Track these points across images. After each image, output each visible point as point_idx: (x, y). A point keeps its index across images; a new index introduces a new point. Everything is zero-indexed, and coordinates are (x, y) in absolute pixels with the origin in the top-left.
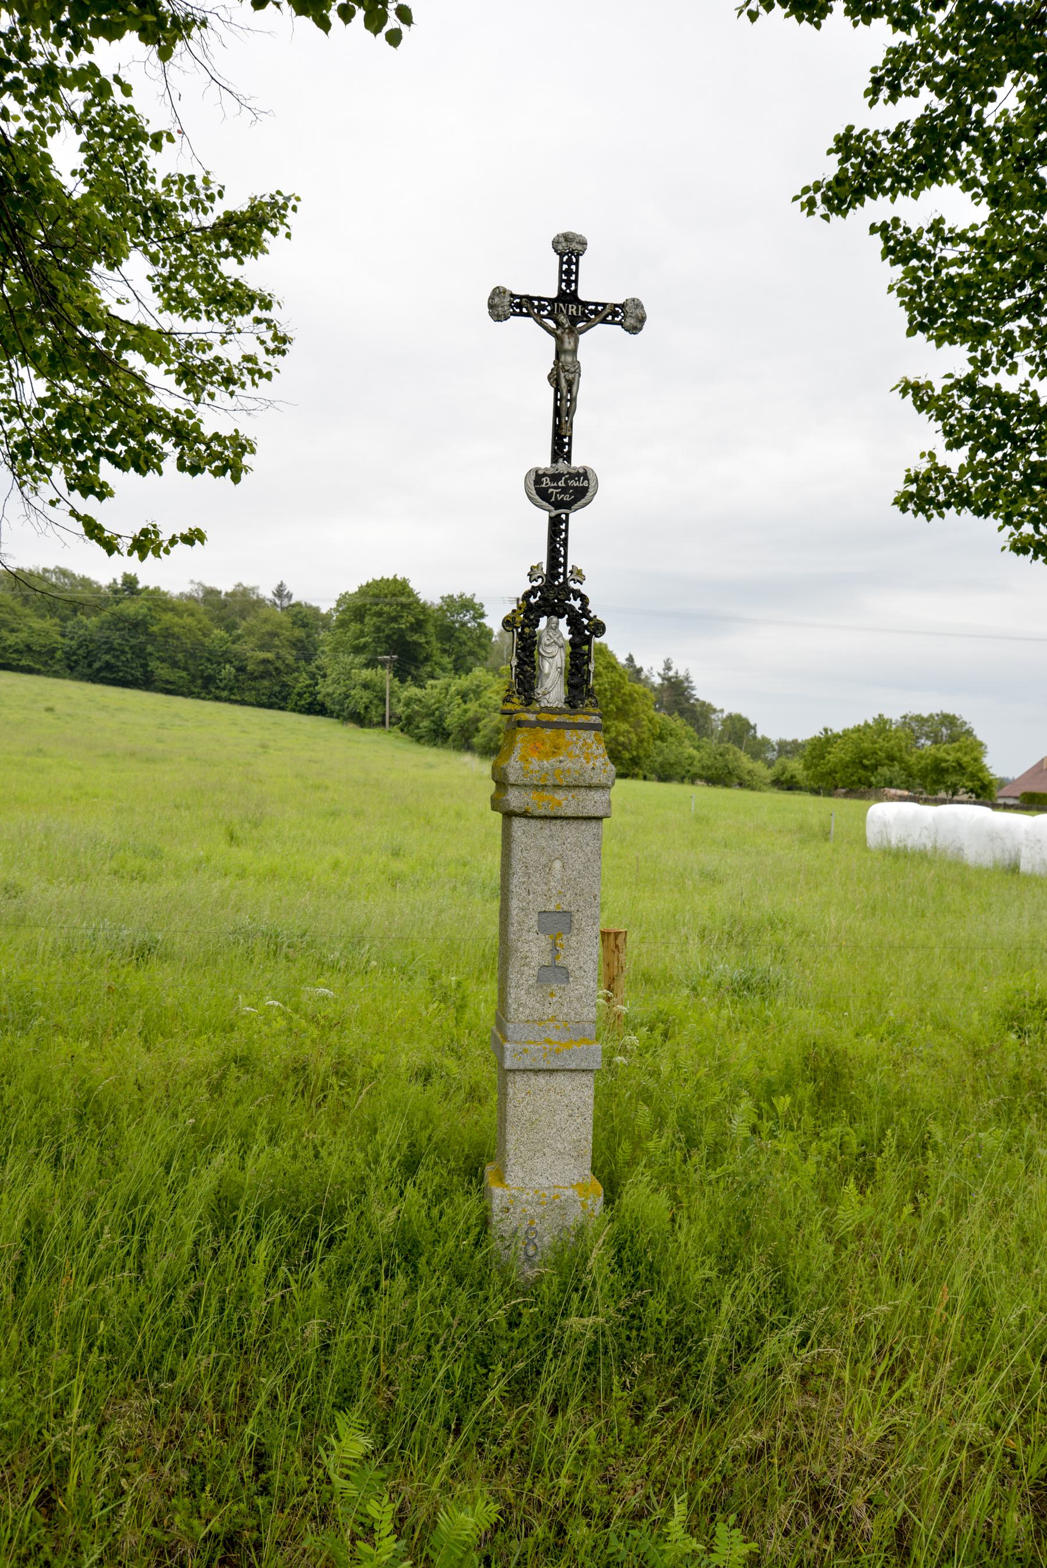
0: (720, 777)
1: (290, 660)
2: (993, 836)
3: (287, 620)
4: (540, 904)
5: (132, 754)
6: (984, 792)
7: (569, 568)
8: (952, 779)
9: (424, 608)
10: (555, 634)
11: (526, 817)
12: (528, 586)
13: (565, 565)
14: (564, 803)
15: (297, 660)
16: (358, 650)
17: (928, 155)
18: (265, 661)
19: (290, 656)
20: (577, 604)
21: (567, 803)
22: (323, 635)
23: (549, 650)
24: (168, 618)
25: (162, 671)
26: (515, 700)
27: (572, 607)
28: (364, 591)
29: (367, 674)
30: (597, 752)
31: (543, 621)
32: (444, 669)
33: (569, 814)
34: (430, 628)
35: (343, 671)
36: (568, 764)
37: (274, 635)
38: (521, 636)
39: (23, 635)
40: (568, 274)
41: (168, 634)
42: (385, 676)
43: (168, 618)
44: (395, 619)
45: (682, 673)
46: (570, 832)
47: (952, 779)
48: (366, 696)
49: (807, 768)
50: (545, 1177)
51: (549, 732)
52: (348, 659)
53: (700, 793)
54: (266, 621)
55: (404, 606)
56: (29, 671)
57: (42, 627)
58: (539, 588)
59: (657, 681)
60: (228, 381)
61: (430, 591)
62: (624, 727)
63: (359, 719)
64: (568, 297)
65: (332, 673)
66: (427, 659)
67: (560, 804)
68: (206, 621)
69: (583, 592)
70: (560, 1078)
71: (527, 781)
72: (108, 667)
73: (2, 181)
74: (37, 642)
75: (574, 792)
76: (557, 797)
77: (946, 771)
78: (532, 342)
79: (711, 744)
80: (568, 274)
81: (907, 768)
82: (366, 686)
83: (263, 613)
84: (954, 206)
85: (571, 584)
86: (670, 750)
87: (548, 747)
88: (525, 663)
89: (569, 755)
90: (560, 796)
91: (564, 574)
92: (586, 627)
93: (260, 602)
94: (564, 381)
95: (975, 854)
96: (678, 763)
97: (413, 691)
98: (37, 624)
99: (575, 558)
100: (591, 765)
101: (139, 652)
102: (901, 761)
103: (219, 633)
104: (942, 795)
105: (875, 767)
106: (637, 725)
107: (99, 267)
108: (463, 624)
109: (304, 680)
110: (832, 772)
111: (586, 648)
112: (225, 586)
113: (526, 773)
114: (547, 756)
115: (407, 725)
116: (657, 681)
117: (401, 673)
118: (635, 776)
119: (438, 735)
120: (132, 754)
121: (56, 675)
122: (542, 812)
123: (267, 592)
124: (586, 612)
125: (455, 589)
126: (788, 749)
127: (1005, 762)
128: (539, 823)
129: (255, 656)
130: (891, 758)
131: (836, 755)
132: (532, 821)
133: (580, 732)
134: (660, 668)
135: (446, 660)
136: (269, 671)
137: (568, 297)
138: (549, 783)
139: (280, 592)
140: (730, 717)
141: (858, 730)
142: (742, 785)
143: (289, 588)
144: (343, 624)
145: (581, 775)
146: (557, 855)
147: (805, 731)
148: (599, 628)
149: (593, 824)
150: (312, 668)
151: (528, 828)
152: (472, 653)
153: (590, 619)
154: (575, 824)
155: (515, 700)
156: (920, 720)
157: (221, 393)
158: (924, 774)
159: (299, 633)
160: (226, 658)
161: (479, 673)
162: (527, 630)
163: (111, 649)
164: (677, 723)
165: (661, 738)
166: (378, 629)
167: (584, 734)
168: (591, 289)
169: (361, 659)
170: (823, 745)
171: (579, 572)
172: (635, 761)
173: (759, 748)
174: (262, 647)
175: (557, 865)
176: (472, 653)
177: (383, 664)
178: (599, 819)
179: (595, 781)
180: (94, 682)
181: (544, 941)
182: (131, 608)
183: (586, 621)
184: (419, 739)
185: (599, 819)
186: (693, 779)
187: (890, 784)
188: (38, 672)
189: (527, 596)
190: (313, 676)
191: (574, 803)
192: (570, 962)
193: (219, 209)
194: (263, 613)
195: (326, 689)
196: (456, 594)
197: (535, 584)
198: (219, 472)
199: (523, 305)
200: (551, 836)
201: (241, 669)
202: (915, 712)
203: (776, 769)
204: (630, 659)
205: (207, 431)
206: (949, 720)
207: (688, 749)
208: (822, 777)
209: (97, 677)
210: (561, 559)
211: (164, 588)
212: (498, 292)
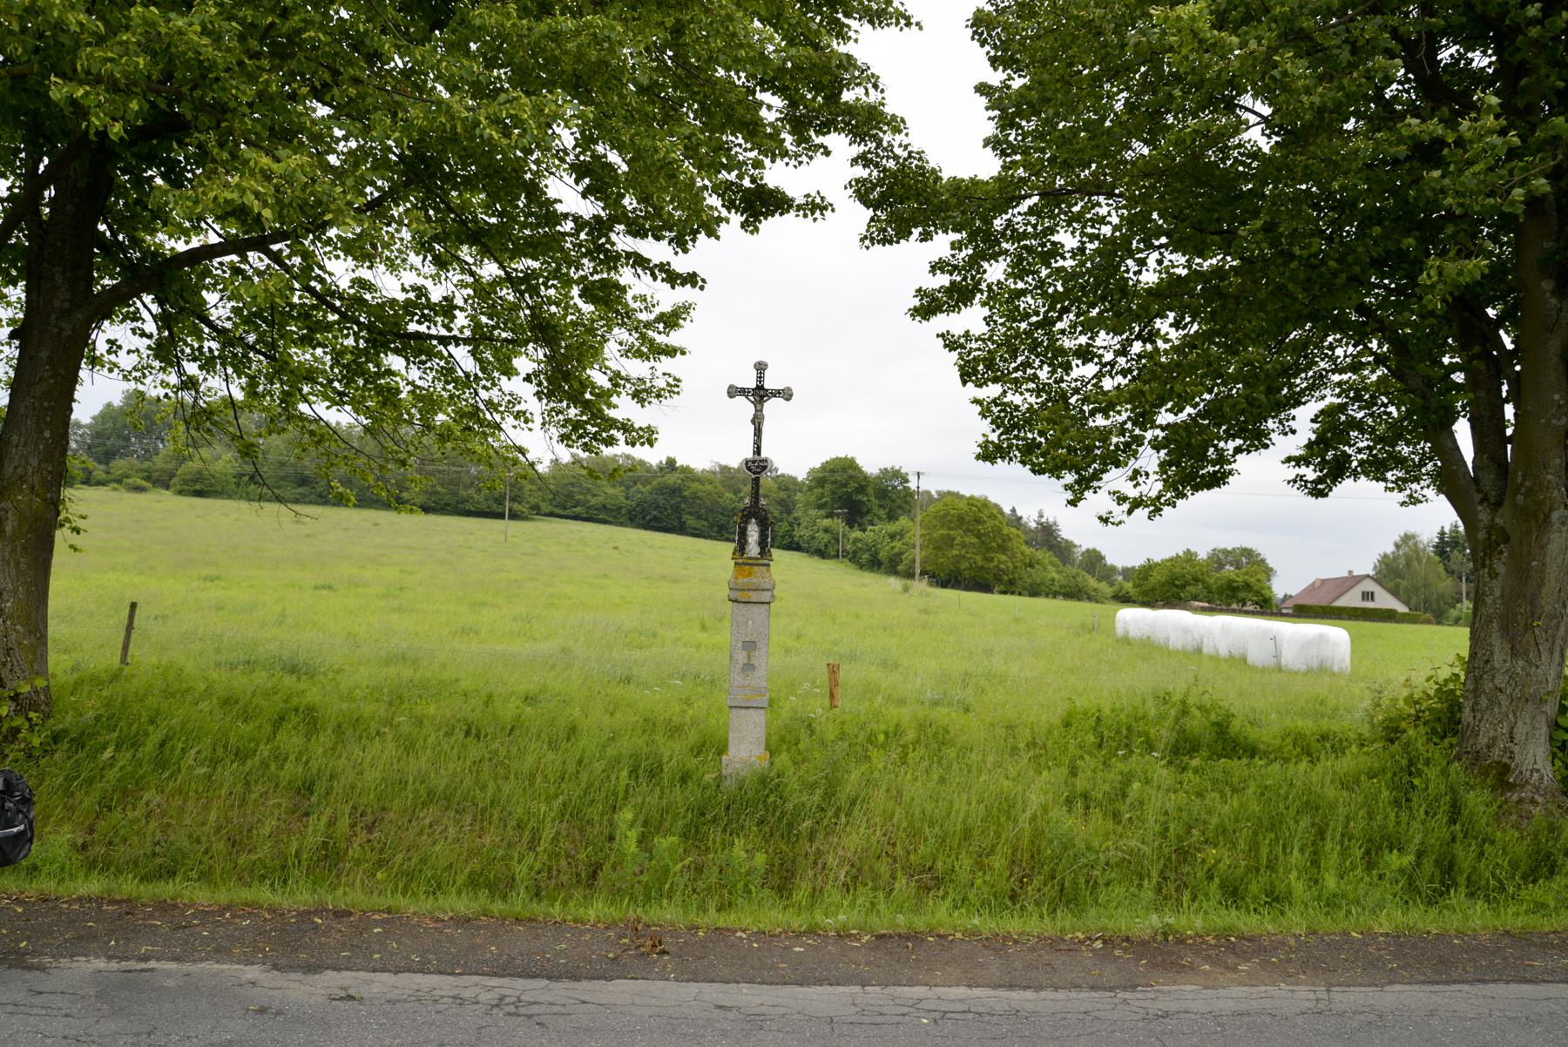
0: (1074, 593)
1: (776, 513)
2: (1186, 630)
3: (775, 486)
4: (743, 638)
5: (664, 577)
6: (1265, 606)
8: (1242, 595)
9: (866, 478)
16: (820, 507)
17: (959, 296)
21: (754, 596)
22: (799, 496)
24: (695, 485)
25: (691, 521)
28: (824, 466)
29: (827, 522)
32: (880, 519)
34: (870, 491)
35: (815, 522)
39: (600, 499)
40: (760, 378)
41: (695, 496)
42: (838, 525)
43: (695, 485)
44: (845, 485)
45: (1051, 520)
46: (755, 608)
47: (1242, 595)
48: (826, 537)
49: (1135, 586)
50: (746, 750)
52: (813, 512)
53: (1060, 604)
55: (851, 477)
56: (605, 522)
57: (611, 493)
59: (1033, 525)
60: (658, 396)
61: (871, 464)
62: (1003, 558)
63: (822, 554)
64: (760, 388)
65: (804, 521)
66: (868, 511)
68: (720, 488)
70: (751, 711)
72: (656, 519)
73: (682, 5)
74: (610, 503)
77: (1237, 589)
78: (745, 407)
79: (1070, 570)
80: (760, 378)
81: (1207, 587)
82: (826, 530)
84: (972, 319)
86: (1036, 575)
94: (757, 422)
95: (1176, 642)
96: (1043, 583)
97: (857, 534)
98: (611, 491)
101: (677, 509)
102: (1203, 582)
103: (729, 495)
104: (1234, 606)
105: (1184, 586)
106: (1013, 557)
108: (894, 487)
109: (785, 526)
110: (1153, 589)
115: (854, 558)
116: (1033, 525)
117: (851, 522)
118: (1013, 593)
119: (874, 564)
120: (664, 577)
121: (622, 524)
125: (888, 464)
126: (1127, 572)
127: (1284, 586)
130: (1196, 580)
131: (1156, 577)
134: (1035, 516)
135: (882, 512)
137: (760, 388)
140: (1088, 551)
141: (1171, 560)
142: (1090, 599)
144: (810, 489)
147: (1136, 561)
150: (790, 519)
152: (900, 507)
156: (1226, 552)
157: (655, 401)
158: (1221, 591)
159: (783, 495)
161: (903, 521)
163: (658, 507)
164: (1043, 555)
165: (1031, 566)
166: (833, 493)
168: (769, 384)
169: (822, 512)
170: (1148, 569)
172: (1012, 582)
173: (1108, 573)
176: (900, 507)
177: (838, 515)
180: (646, 528)
181: (745, 653)
182: (671, 479)
184: (861, 567)
186: (1055, 595)
187: (1195, 598)
188: (610, 523)
190: (791, 525)
192: (755, 663)
193: (657, 311)
195: (801, 533)
196: (889, 467)
198: (642, 444)
199: (743, 392)
202: (1222, 546)
203: (1116, 588)
204: (1014, 510)
205: (637, 426)
206: (1248, 553)
207: (1053, 573)
208: (1146, 593)
209: (647, 526)
211: (692, 466)
212: (731, 387)
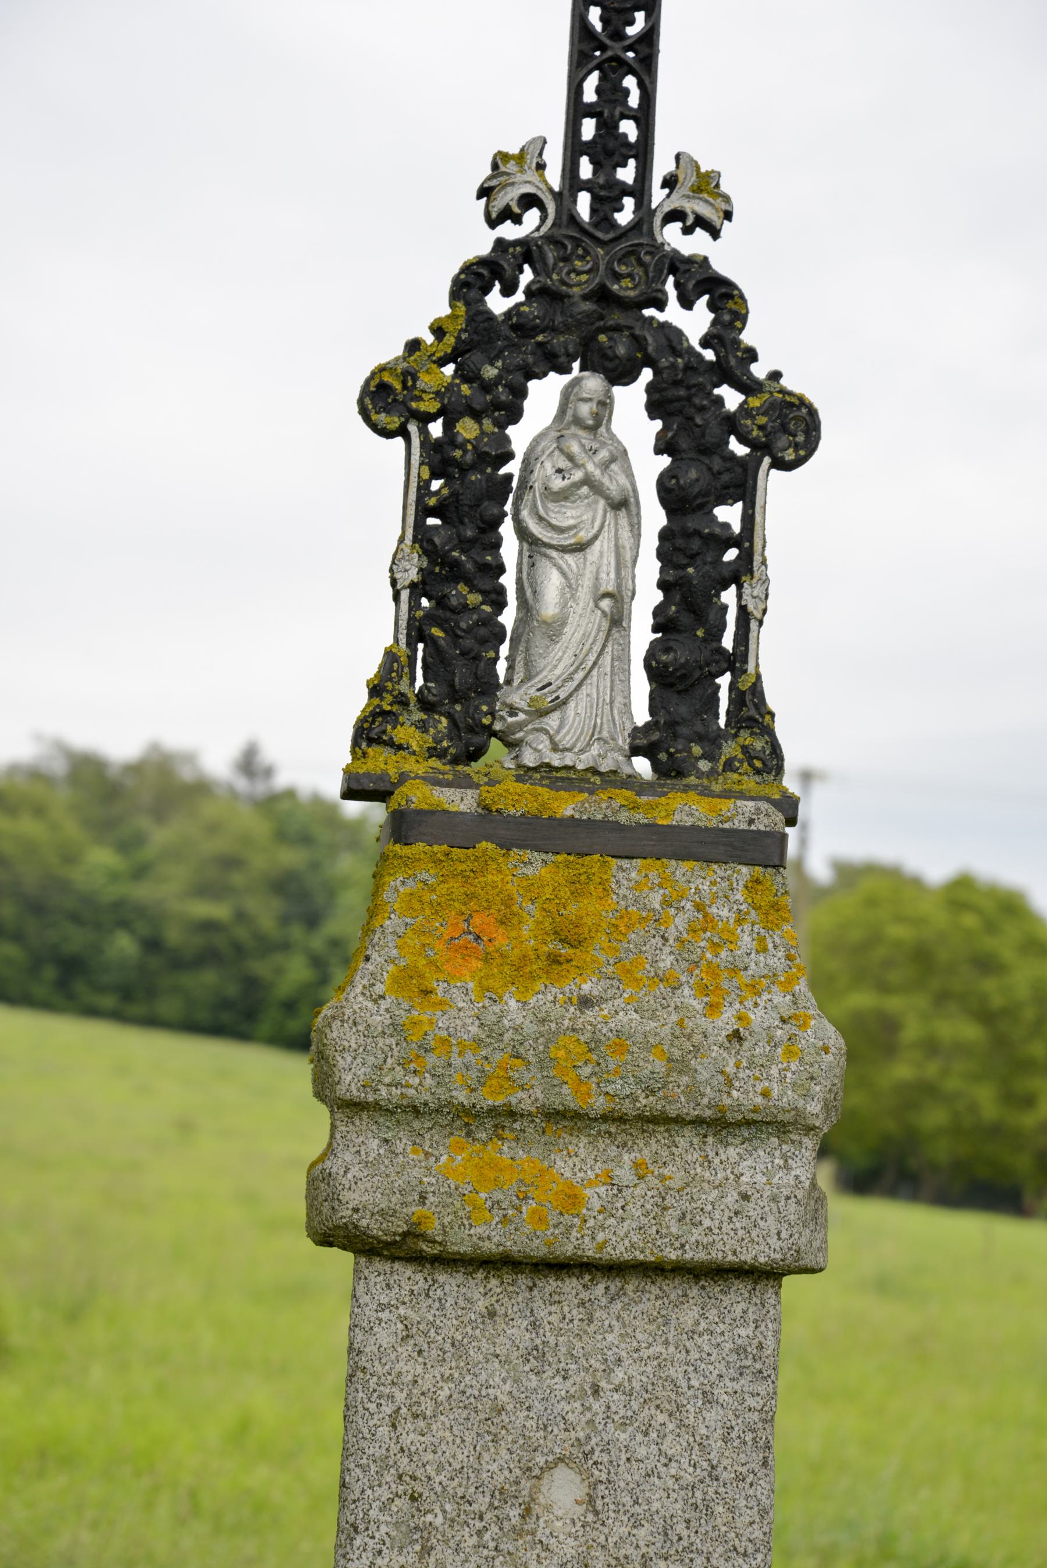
3: (261, 828)
7: (662, 165)
10: (593, 441)
11: (417, 1259)
12: (480, 242)
13: (643, 151)
14: (595, 1196)
15: (285, 920)
18: (209, 926)
19: (266, 913)
20: (694, 322)
23: (566, 515)
26: (405, 733)
27: (672, 335)
30: (757, 965)
31: (544, 395)
33: (619, 1251)
36: (619, 1015)
37: (231, 863)
38: (439, 458)
46: (625, 1332)
51: (537, 867)
54: (213, 828)
58: (527, 251)
67: (572, 1199)
69: (721, 266)
71: (421, 1088)
75: (647, 1148)
76: (563, 1166)
83: (209, 810)
85: (672, 236)
87: (529, 934)
88: (455, 573)
89: (623, 973)
90: (578, 1163)
91: (640, 190)
92: (732, 424)
93: (202, 788)
99: (689, 118)
100: (726, 1019)
103: (102, 857)
107: (425, 564)
111: (729, 515)
112: (120, 745)
113: (415, 1047)
114: (521, 973)
122: (488, 1235)
123: (218, 762)
124: (732, 358)
128: (477, 1292)
129: (178, 901)
132: (449, 1282)
133: (682, 869)
136: (215, 947)
138: (523, 1100)
139: (249, 763)
143: (270, 753)
145: (679, 1065)
146: (560, 1443)
148: (790, 429)
149: (737, 1299)
151: (424, 1312)
153: (748, 386)
154: (648, 1299)
155: (405, 733)
159: (290, 857)
160: (122, 915)
162: (467, 429)
167: (699, 880)
171: (707, 184)
174: (204, 890)
175: (563, 1491)
178: (764, 1276)
179: (745, 1097)
183: (732, 398)
185: (764, 1276)
189: (472, 281)
191: (640, 1196)
194: (209, 810)
197: (509, 231)
200: (537, 1354)
201: (152, 945)
210: (629, 128)
